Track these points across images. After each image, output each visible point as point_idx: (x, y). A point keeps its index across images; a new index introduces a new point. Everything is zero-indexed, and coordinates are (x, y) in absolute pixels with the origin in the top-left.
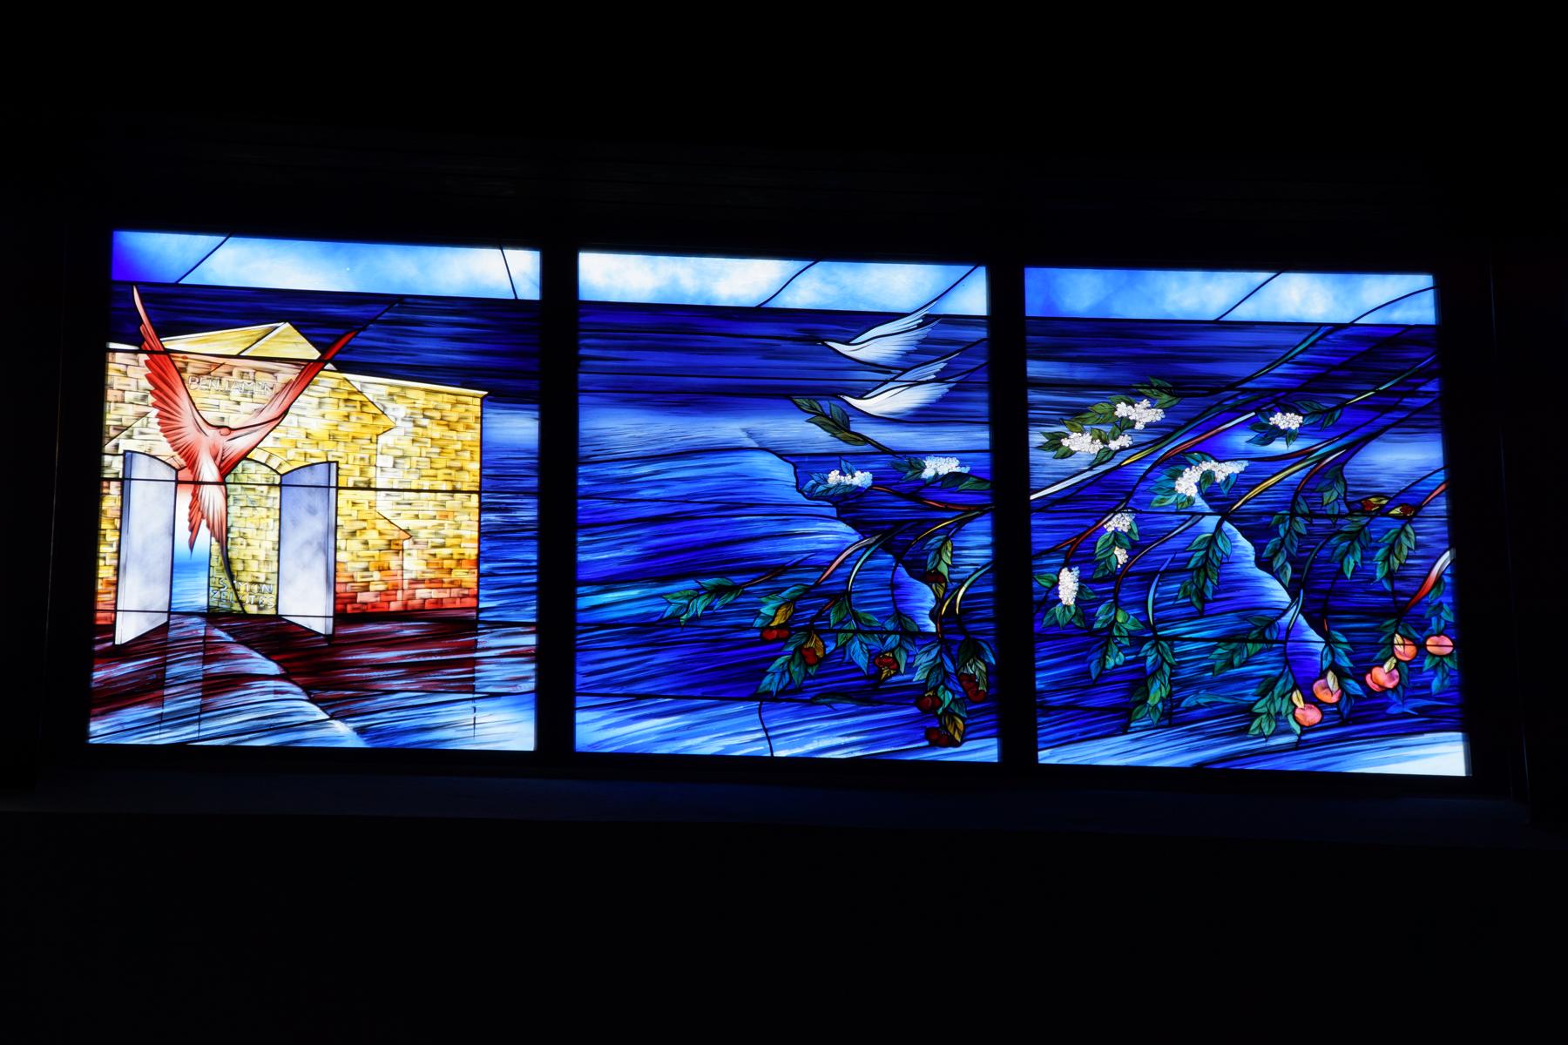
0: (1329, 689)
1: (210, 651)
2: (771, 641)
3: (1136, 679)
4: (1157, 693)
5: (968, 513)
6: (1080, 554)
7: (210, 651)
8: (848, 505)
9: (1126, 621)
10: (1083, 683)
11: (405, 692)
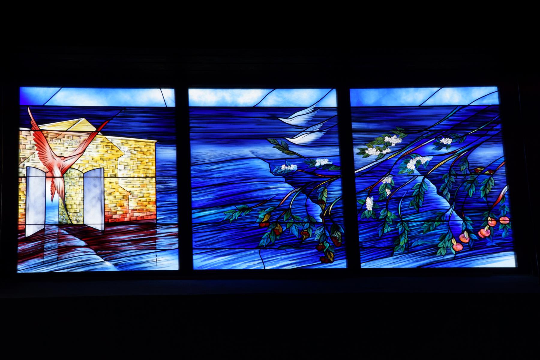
0: (465, 237)
1: (60, 238)
2: (263, 227)
3: (395, 236)
4: (403, 241)
5: (332, 179)
6: (373, 192)
7: (60, 238)
8: (289, 177)
9: (391, 215)
10: (376, 239)
11: (131, 250)
